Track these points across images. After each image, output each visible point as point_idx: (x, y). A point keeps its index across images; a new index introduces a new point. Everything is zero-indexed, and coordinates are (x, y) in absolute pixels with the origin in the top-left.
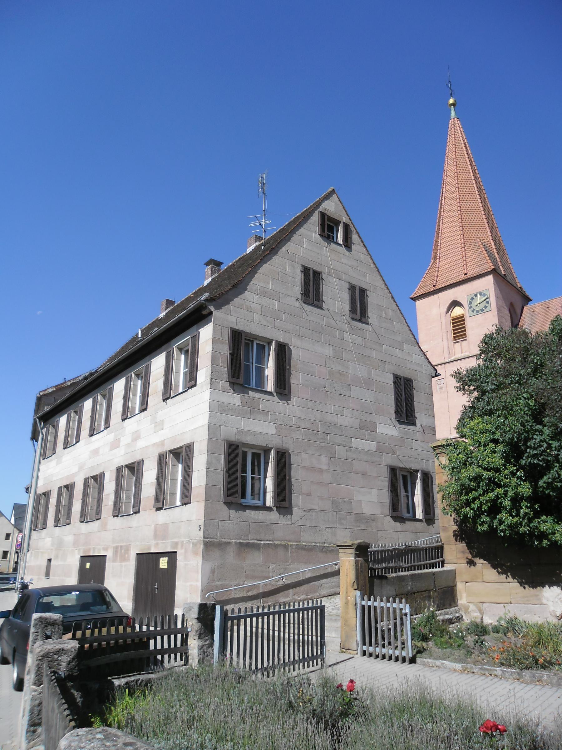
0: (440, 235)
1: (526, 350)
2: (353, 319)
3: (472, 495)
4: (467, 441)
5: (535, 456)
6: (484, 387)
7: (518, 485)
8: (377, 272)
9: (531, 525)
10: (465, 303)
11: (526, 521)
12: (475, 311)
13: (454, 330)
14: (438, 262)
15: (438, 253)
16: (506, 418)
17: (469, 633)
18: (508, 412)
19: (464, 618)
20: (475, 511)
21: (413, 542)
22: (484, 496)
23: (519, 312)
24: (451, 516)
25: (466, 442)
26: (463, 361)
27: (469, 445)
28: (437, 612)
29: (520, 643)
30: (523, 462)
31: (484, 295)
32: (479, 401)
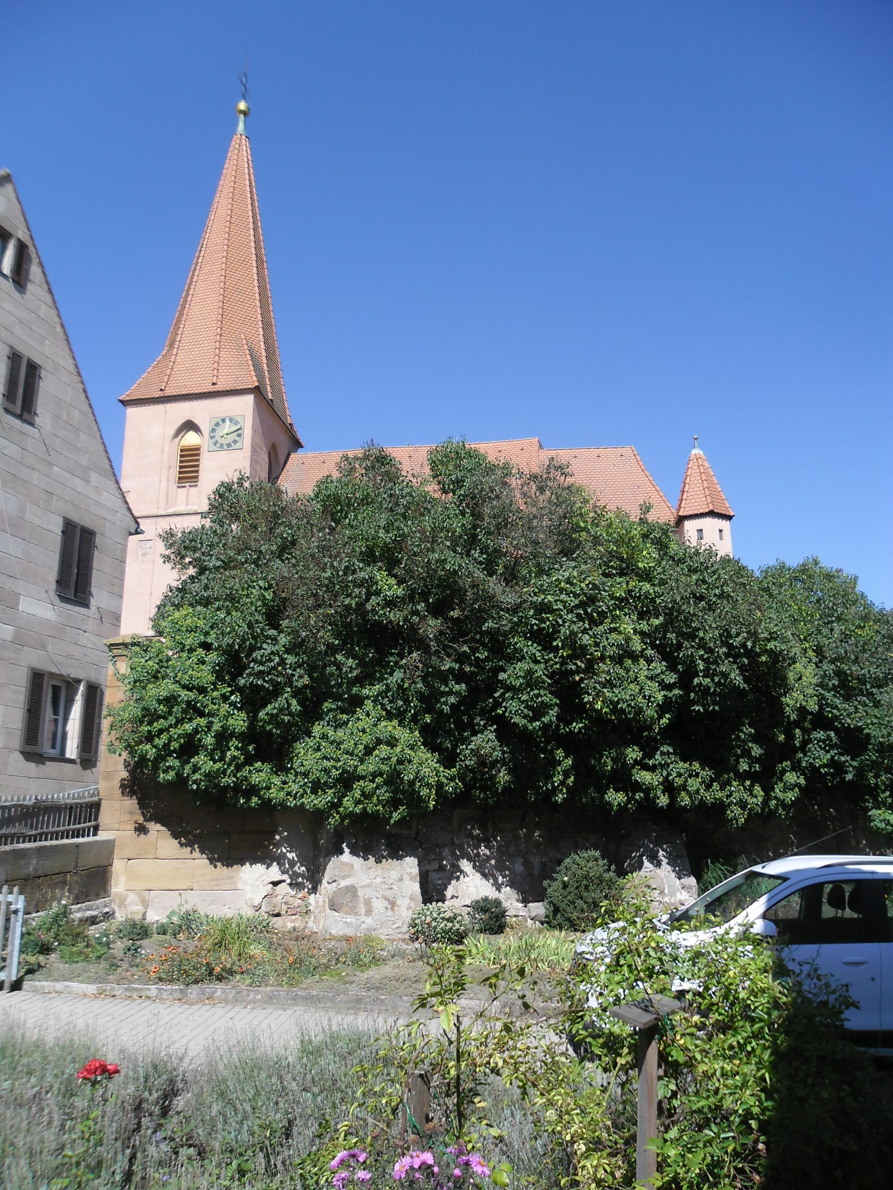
0: (185, 312)
1: (276, 516)
2: (7, 411)
3: (161, 724)
4: (163, 640)
5: (260, 674)
6: (204, 561)
7: (229, 715)
8: (65, 343)
9: (239, 775)
10: (205, 428)
11: (232, 768)
12: (219, 445)
13: (180, 467)
14: (174, 353)
15: (178, 339)
16: (229, 613)
17: (120, 937)
18: (233, 605)
19: (117, 915)
20: (159, 750)
21: (56, 796)
22: (176, 727)
23: (282, 460)
24: (120, 755)
25: (162, 643)
26: (186, 517)
27: (167, 647)
28: (74, 907)
29: (191, 946)
30: (242, 682)
31: (236, 423)
32: (194, 582)
